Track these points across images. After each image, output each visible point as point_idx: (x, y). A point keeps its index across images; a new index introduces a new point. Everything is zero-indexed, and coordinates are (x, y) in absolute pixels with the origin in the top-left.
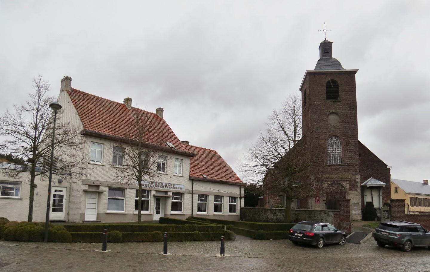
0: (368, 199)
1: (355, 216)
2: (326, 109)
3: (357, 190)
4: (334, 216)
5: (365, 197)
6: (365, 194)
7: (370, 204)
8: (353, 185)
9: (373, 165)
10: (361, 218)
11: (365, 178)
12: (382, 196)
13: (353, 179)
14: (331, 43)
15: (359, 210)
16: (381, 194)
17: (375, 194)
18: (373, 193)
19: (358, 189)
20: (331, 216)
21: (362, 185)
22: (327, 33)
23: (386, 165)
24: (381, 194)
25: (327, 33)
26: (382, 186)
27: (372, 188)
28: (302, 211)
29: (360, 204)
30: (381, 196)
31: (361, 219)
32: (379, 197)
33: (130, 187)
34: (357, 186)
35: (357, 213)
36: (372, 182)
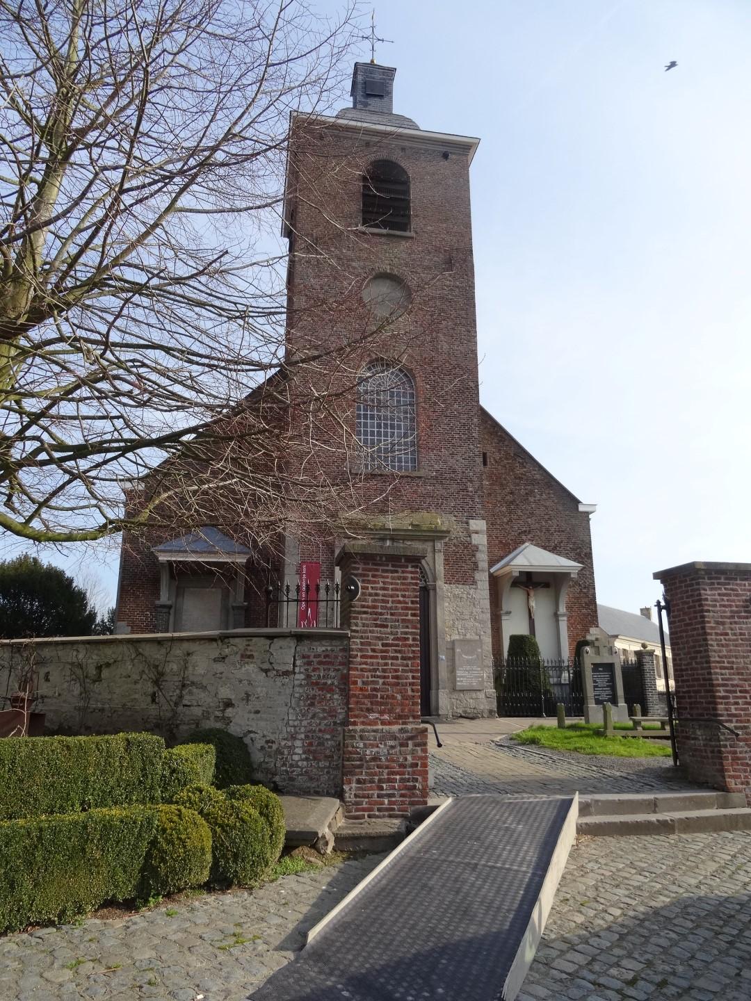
0: (514, 626)
1: (467, 696)
2: (359, 258)
3: (474, 583)
4: (308, 677)
5: (503, 618)
6: (505, 608)
7: (522, 645)
8: (462, 568)
9: (532, 499)
10: (494, 706)
11: (504, 545)
12: (565, 618)
13: (457, 531)
14: (390, 72)
15: (483, 667)
16: (562, 609)
17: (540, 604)
18: (533, 603)
19: (478, 576)
20: (286, 673)
21: (492, 570)
22: (378, 45)
23: (576, 502)
24: (562, 609)
25: (378, 45)
26: (569, 574)
27: (530, 581)
28: (143, 645)
29: (488, 640)
30: (563, 615)
31: (491, 712)
32: (557, 621)
33: (587, 721)
34: (476, 564)
35: (475, 684)
36: (532, 557)
